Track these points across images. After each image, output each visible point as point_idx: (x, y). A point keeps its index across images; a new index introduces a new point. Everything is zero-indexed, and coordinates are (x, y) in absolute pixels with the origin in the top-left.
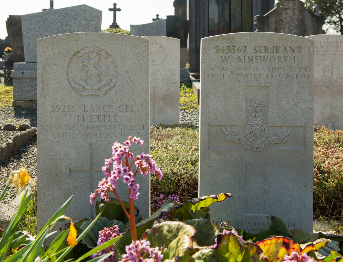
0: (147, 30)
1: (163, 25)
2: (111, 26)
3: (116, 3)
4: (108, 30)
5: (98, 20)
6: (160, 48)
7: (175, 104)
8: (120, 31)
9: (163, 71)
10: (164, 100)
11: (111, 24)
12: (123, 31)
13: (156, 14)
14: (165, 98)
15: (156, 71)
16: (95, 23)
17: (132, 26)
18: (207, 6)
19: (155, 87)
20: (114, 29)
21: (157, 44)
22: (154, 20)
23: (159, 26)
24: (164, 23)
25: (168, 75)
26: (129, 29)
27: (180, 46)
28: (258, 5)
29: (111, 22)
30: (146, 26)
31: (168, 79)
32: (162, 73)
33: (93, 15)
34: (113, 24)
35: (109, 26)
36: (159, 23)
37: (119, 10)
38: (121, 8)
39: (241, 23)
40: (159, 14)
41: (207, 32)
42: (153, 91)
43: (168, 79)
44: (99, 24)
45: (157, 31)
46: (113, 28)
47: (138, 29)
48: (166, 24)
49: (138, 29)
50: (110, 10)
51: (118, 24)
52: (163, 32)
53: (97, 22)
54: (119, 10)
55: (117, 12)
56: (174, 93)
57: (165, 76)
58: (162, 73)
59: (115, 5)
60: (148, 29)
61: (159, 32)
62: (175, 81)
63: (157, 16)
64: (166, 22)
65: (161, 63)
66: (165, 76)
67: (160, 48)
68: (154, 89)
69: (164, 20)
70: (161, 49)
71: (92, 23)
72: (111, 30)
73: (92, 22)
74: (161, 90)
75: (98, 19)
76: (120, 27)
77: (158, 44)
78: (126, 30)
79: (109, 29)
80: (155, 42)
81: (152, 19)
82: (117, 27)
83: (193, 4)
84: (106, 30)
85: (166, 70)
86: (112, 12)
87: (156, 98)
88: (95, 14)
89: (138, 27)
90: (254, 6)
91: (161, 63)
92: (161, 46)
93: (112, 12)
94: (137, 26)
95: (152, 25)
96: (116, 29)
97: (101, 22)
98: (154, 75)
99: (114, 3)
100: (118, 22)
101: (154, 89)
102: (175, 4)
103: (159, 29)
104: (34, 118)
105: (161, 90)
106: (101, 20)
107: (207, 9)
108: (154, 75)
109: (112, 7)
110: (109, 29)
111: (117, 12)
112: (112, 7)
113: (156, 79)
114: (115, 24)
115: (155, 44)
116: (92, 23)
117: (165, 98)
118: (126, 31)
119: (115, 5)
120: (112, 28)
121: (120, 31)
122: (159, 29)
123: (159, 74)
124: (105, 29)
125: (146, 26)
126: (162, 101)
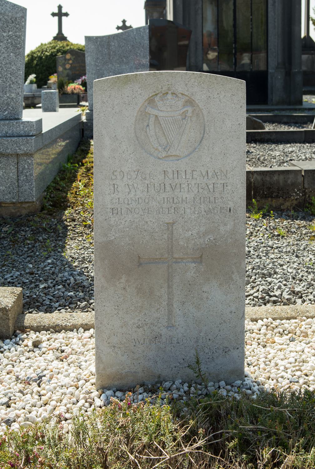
0: (114, 45)
1: (143, 37)
2: (55, 38)
3: (62, 5)
4: (50, 43)
5: (17, 28)
6: (184, 106)
7: (233, 273)
8: (67, 45)
9: (195, 176)
10: (199, 260)
11: (55, 35)
12: (72, 44)
13: (122, 20)
14: (201, 257)
15: (176, 175)
16: (10, 33)
17: (88, 39)
18: (200, 6)
19: (173, 223)
20: (59, 42)
21: (177, 96)
22: (118, 28)
23: (136, 38)
24: (145, 32)
25: (211, 187)
26: (82, 42)
27: (245, 101)
28: (276, 4)
29: (55, 32)
30: (114, 38)
31: (212, 199)
32: (193, 182)
33: (6, 17)
34: (57, 34)
35: (52, 38)
36: (137, 33)
37: (66, 15)
38: (69, 13)
39: (252, 33)
40: (126, 20)
41: (201, 45)
42: (165, 236)
43: (212, 199)
44: (19, 37)
45: (133, 46)
46: (58, 41)
47: (98, 43)
48: (148, 34)
49: (98, 43)
50: (54, 15)
51: (65, 35)
52: (143, 48)
53: (16, 32)
54: (66, 15)
55: (64, 18)
56: (230, 240)
57: (201, 191)
58: (193, 182)
59: (60, 7)
60: (117, 43)
61: (137, 49)
62: (231, 205)
63: (124, 22)
64: (148, 31)
65: (191, 153)
66: (201, 191)
67: (184, 106)
68: (168, 229)
69: (143, 28)
70: (190, 109)
71: (5, 34)
72: (55, 43)
73: (5, 32)
74: (190, 232)
75: (18, 26)
76: (68, 39)
77: (180, 95)
78: (76, 43)
79: (53, 43)
80: (169, 89)
81: (117, 26)
82: (64, 39)
83: (179, 3)
84: (48, 44)
85: (204, 173)
86: (56, 18)
87: (176, 256)
88: (10, 14)
89: (99, 40)
90: (270, 6)
91: (191, 153)
92: (190, 102)
93: (56, 18)
94: (97, 38)
95: (124, 36)
96: (62, 42)
97: (25, 32)
98: (168, 188)
99: (58, 5)
100: (65, 32)
101: (168, 229)
102: (148, 6)
103: (136, 42)
104: (6, 112)
105: (190, 232)
106: (24, 27)
107: (200, 12)
108: (168, 188)
109: (56, 11)
110: (53, 43)
111: (64, 18)
112: (56, 11)
113: (176, 200)
114: (61, 35)
115: (169, 96)
116: (5, 34)
117: (201, 257)
118: (77, 44)
119: (60, 7)
120: (56, 41)
121: (67, 45)
122: (136, 42)
123: (183, 186)
124: (47, 43)
125: (114, 38)
126: (194, 265)
